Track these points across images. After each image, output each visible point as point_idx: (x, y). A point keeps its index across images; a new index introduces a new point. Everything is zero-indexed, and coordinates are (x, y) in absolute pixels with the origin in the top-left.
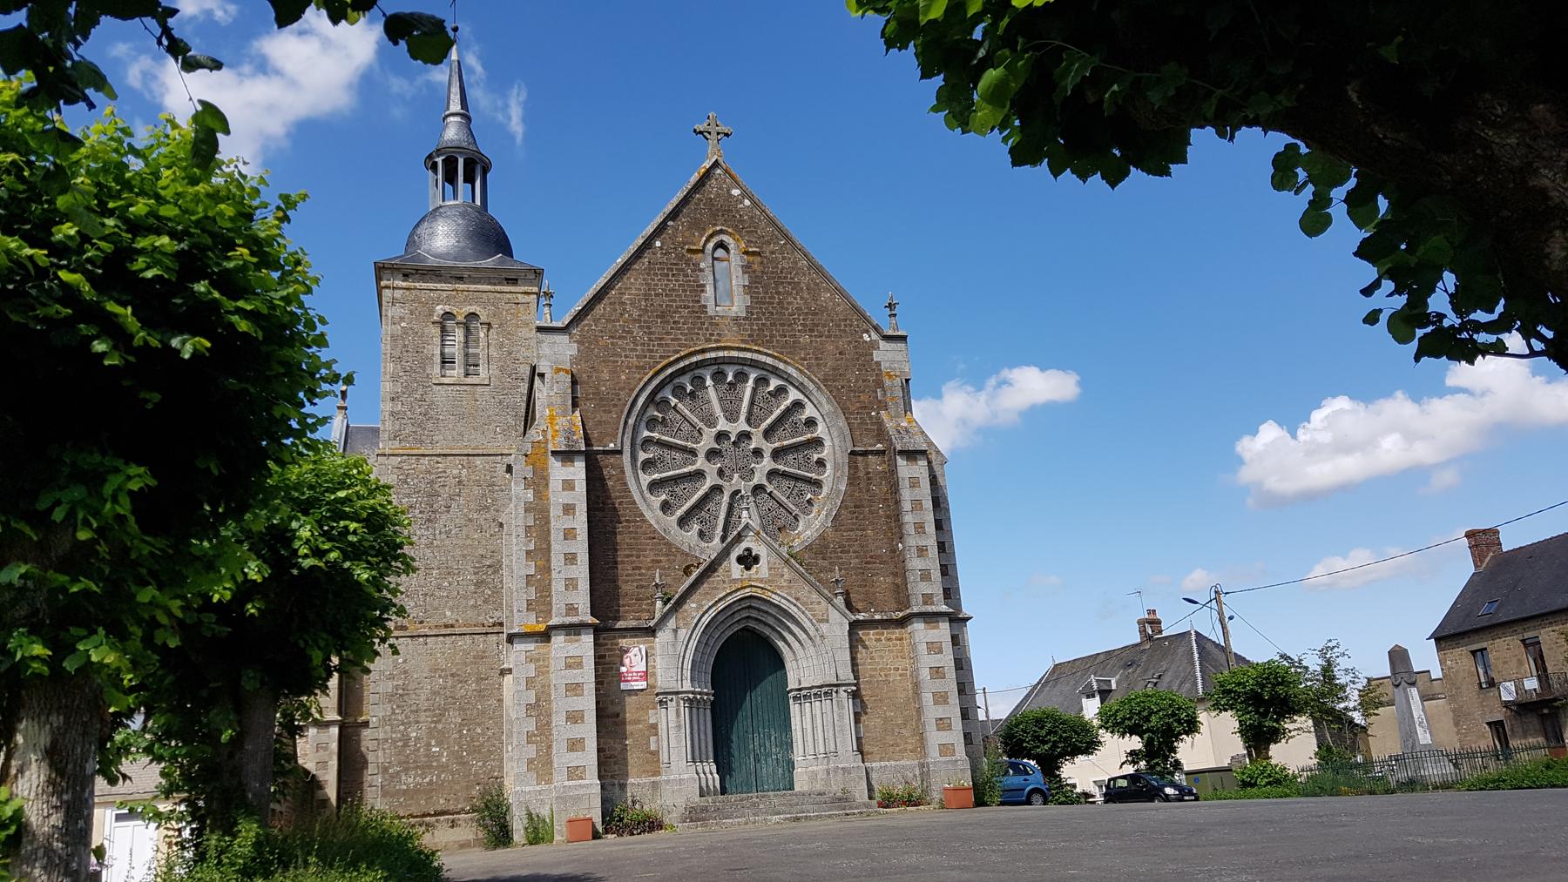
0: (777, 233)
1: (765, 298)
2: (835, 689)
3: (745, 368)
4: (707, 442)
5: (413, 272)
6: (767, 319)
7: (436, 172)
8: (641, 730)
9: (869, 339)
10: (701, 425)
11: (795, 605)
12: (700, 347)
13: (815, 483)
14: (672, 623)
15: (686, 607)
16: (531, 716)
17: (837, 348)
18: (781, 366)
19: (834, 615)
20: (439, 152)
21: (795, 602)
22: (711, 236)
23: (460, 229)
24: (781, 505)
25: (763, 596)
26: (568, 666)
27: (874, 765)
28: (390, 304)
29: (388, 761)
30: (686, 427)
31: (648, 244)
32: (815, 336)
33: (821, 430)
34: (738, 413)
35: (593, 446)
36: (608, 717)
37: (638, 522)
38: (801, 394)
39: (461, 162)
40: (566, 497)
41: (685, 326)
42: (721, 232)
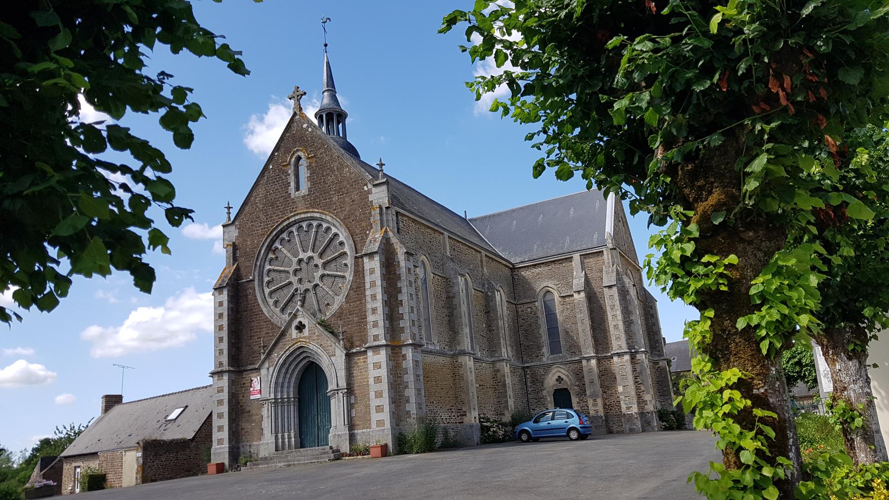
2: (336, 392)
3: (289, 229)
8: (258, 418)
13: (289, 284)
14: (266, 365)
15: (273, 356)
17: (351, 198)
18: (324, 217)
22: (293, 154)
26: (219, 392)
27: (360, 431)
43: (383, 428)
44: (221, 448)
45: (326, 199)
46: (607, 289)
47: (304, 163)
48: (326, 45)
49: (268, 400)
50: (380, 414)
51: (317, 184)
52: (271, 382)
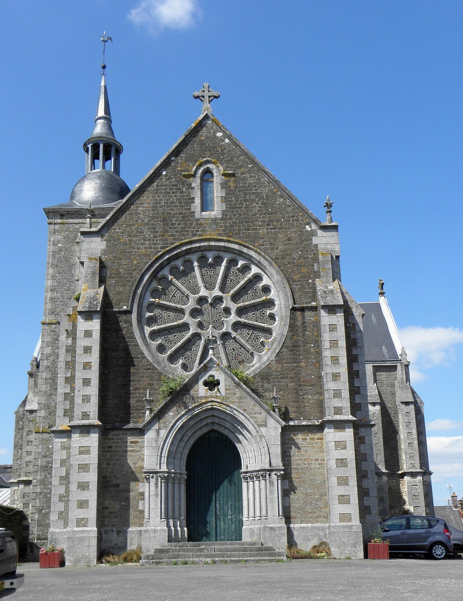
0: (247, 160)
1: (236, 204)
3: (221, 253)
4: (191, 304)
5: (66, 213)
6: (236, 219)
7: (88, 154)
9: (310, 229)
10: (187, 292)
11: (243, 415)
12: (189, 240)
14: (156, 427)
16: (62, 484)
17: (287, 236)
18: (245, 250)
19: (271, 422)
20: (89, 141)
21: (242, 412)
22: (200, 165)
23: (97, 186)
24: (241, 346)
25: (220, 408)
26: (81, 453)
27: (296, 525)
28: (53, 233)
29: (42, 505)
30: (178, 294)
31: (156, 174)
32: (271, 228)
33: (273, 295)
34: (215, 284)
35: (113, 308)
36: (112, 486)
37: (139, 358)
38: (260, 270)
39: (101, 146)
40: (86, 342)
41: (179, 226)
42: (208, 162)
43: (350, 524)
44: (84, 531)
45: (249, 230)
46: (404, 405)
47: (217, 179)
48: (104, 67)
49: (157, 473)
50: (345, 506)
51: (235, 208)
52: (163, 449)
